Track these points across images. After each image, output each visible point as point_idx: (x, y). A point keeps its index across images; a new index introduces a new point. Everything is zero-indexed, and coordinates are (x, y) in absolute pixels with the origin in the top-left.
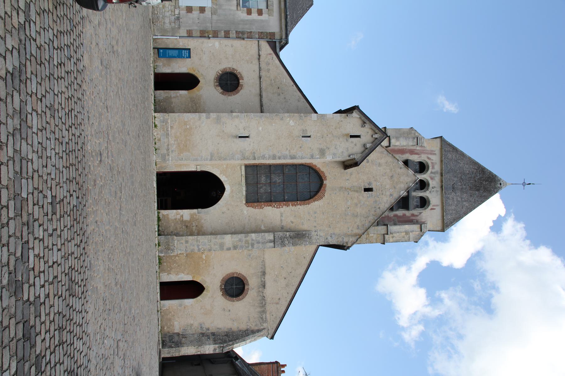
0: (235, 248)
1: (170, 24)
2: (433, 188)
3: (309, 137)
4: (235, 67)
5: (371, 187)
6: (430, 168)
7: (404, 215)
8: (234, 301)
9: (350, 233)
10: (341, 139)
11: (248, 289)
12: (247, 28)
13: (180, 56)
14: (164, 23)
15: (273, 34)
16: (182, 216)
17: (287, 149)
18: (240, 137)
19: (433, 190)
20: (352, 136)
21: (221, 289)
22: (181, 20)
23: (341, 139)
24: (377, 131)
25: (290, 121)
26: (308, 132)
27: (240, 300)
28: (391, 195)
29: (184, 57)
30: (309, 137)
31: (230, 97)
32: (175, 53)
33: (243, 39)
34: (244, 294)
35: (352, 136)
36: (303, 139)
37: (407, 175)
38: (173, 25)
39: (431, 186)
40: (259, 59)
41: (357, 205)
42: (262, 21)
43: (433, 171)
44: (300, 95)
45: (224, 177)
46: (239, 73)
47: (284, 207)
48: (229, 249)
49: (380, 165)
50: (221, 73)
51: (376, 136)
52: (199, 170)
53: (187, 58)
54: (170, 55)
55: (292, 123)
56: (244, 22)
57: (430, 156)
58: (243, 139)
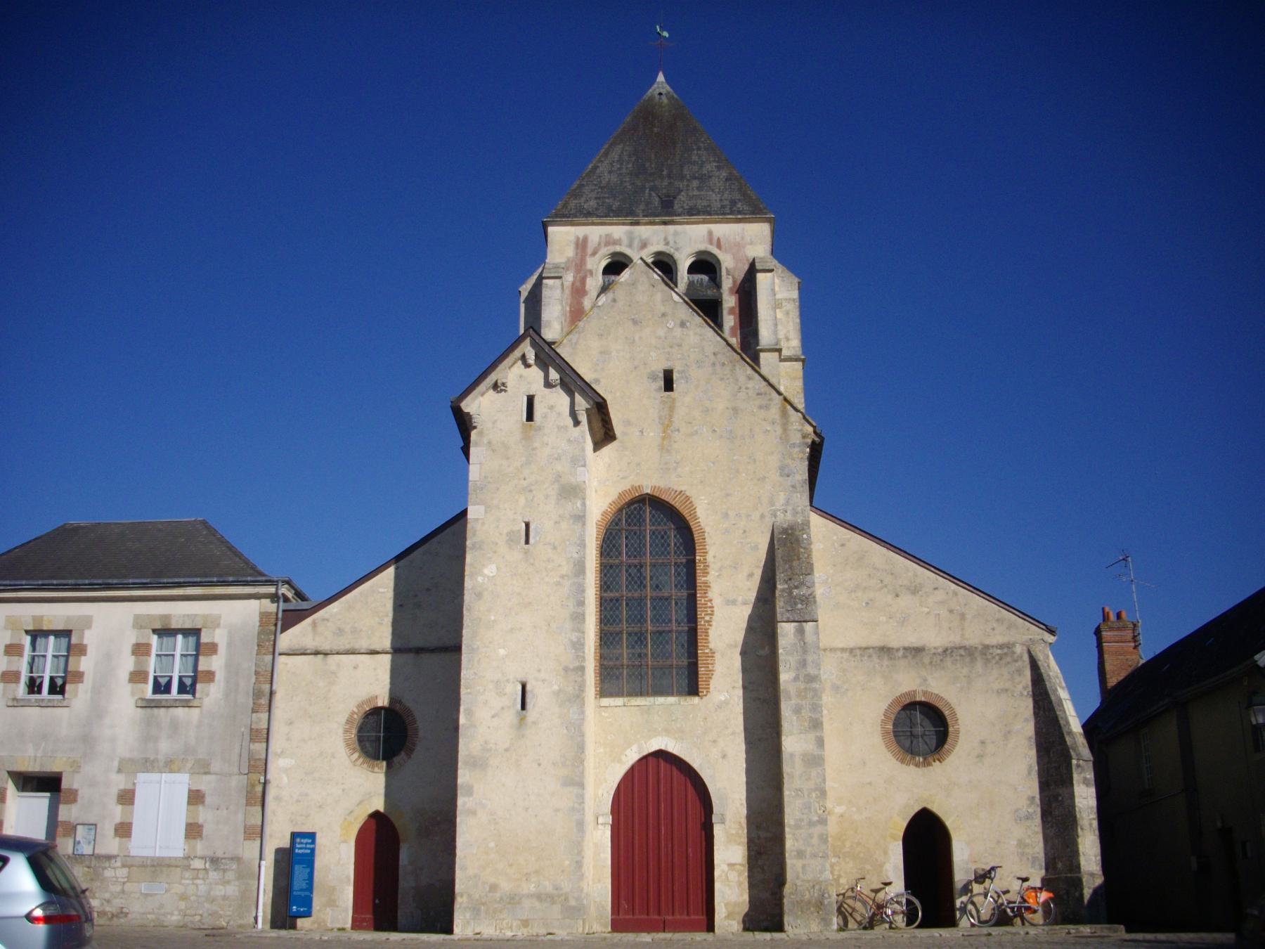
0: (816, 725)
1: (228, 882)
2: (667, 244)
3: (527, 525)
4: (343, 718)
5: (662, 375)
6: (618, 249)
7: (732, 329)
8: (957, 732)
9: (779, 430)
10: (536, 444)
11: (925, 693)
13: (309, 860)
14: (225, 898)
15: (264, 616)
16: (731, 865)
17: (558, 584)
18: (523, 707)
19: (672, 243)
20: (530, 417)
21: (926, 764)
22: (219, 854)
23: (536, 444)
24: (517, 353)
25: (484, 576)
26: (516, 528)
27: (954, 714)
28: (683, 324)
29: (313, 850)
30: (527, 525)
31: (421, 733)
32: (299, 872)
33: (272, 693)
34: (940, 705)
35: (530, 417)
36: (531, 540)
37: (634, 284)
38: (230, 875)
39: (661, 248)
40: (326, 654)
41: (707, 410)
44: (420, 550)
45: (628, 752)
46: (359, 706)
47: (710, 595)
48: (820, 742)
49: (605, 352)
50: (356, 755)
51: (531, 358)
52: (610, 819)
53: (313, 842)
54: (304, 886)
55: (490, 570)
57: (589, 251)
58: (528, 700)
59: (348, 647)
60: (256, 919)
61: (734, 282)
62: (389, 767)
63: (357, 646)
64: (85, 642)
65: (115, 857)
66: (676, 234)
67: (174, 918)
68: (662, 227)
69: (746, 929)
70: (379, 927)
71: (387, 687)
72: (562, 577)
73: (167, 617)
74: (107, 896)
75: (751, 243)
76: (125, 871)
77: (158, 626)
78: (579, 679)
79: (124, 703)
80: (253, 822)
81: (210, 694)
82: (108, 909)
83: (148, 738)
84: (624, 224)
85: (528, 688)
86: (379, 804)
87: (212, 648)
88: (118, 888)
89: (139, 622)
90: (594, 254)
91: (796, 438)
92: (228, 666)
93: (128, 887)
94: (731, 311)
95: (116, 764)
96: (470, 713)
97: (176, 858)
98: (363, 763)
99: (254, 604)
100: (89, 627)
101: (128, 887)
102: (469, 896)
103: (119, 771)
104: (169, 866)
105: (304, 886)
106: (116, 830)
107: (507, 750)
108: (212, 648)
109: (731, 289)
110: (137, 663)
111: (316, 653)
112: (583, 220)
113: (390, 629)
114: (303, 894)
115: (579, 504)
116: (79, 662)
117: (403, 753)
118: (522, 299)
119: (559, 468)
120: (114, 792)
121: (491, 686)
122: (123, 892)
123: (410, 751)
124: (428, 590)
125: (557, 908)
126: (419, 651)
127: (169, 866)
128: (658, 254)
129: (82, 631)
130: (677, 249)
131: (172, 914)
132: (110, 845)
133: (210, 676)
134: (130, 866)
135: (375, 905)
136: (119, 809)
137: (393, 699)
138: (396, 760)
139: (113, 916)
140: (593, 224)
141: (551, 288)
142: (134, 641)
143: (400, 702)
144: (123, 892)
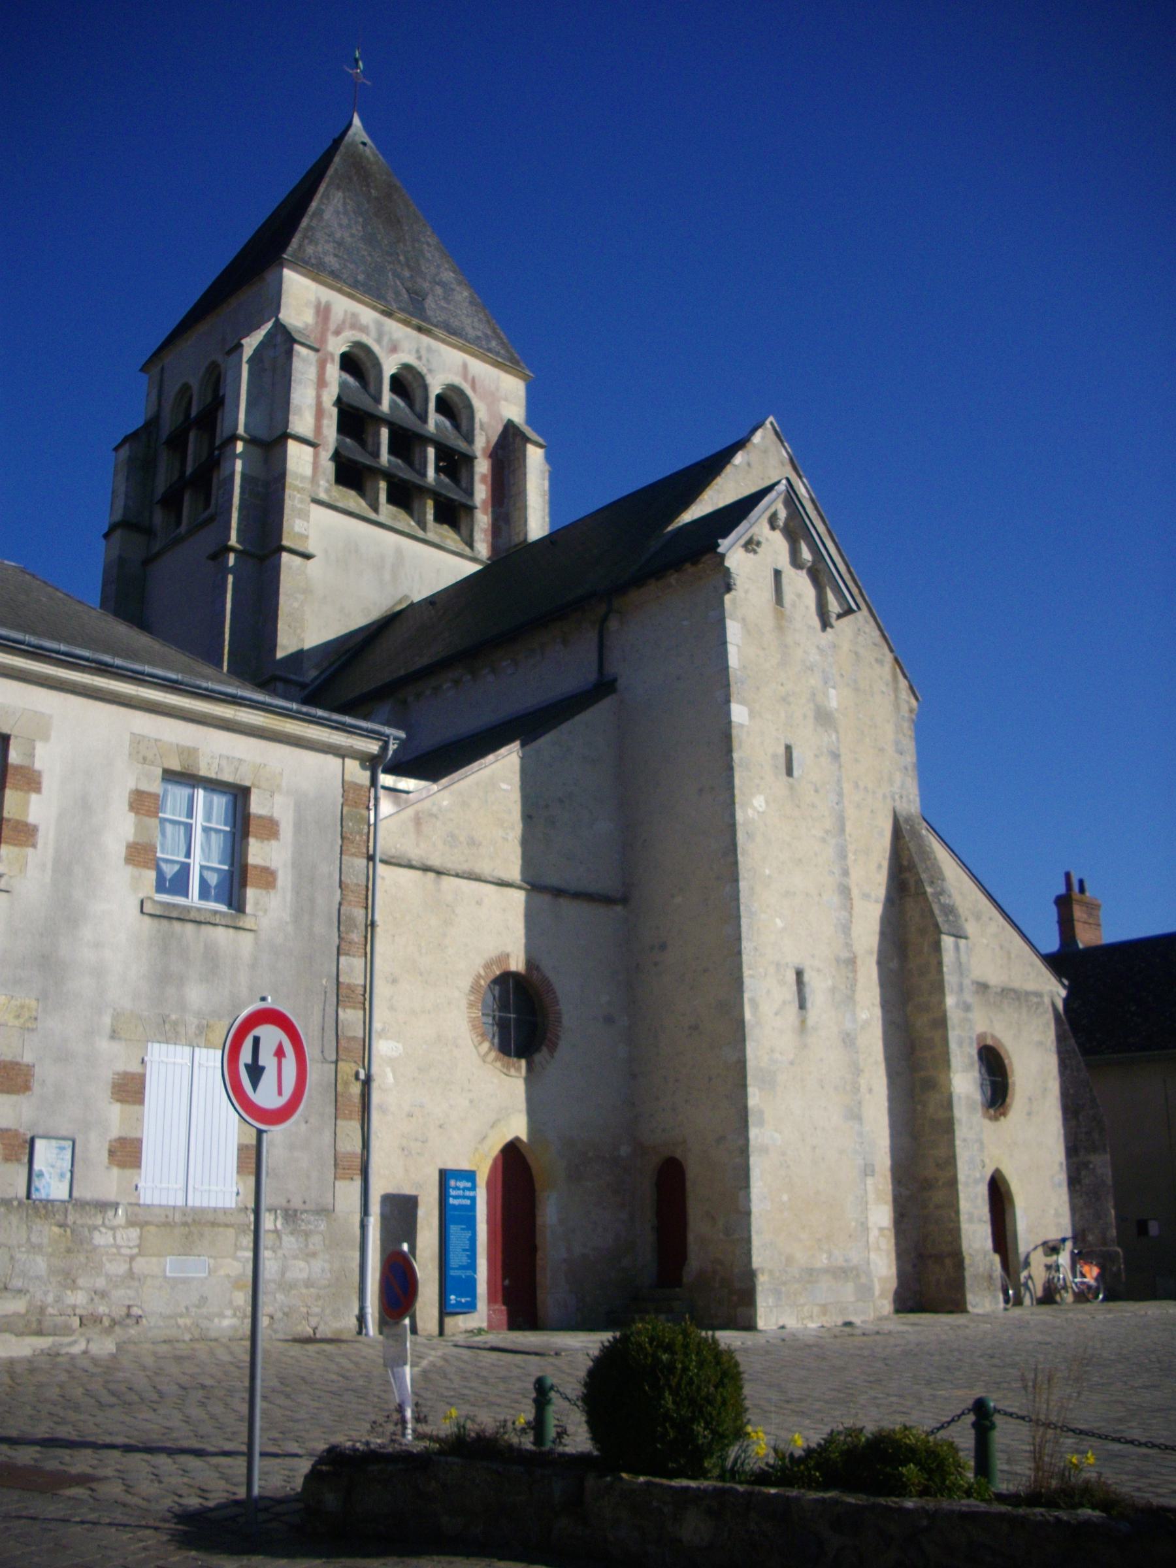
1: (314, 1255)
4: (466, 983)
12: (327, 899)
14: (308, 1284)
18: (802, 1006)
19: (424, 359)
22: (296, 1203)
25: (755, 809)
30: (788, 748)
31: (566, 1020)
38: (316, 1241)
39: (410, 359)
40: (439, 873)
42: (299, 827)
43: (373, 333)
50: (486, 1046)
54: (465, 1261)
55: (759, 802)
56: (303, 909)
57: (332, 326)
59: (464, 867)
60: (361, 1319)
61: (488, 442)
62: (530, 1069)
63: (477, 870)
64: (38, 766)
65: (116, 1206)
66: (429, 349)
67: (226, 1323)
68: (414, 333)
69: (898, 1311)
70: (513, 1325)
71: (522, 941)
72: (827, 832)
73: (190, 753)
74: (101, 1283)
75: (506, 400)
76: (134, 1233)
77: (175, 766)
78: (851, 975)
79: (118, 902)
80: (349, 1149)
81: (268, 907)
82: (102, 1309)
83: (164, 979)
84: (374, 308)
85: (806, 977)
86: (518, 1127)
87: (271, 829)
88: (122, 1268)
89: (140, 749)
90: (337, 333)
91: (905, 709)
92: (298, 864)
93: (140, 1265)
94: (484, 477)
95: (107, 1020)
96: (755, 1005)
97: (225, 1211)
98: (496, 1060)
99: (332, 763)
100: (46, 738)
101: (140, 1265)
102: (771, 1272)
103: (114, 1035)
104: (214, 1224)
105: (465, 1261)
106: (111, 1153)
107: (792, 1063)
108: (271, 829)
109: (484, 450)
110: (139, 828)
111: (426, 869)
112: (330, 281)
113: (518, 850)
114: (463, 1274)
115: (834, 737)
116: (26, 804)
117: (544, 1049)
118: (245, 358)
119: (812, 682)
120: (106, 1075)
121: (772, 970)
122: (131, 1274)
123: (553, 1048)
124: (561, 801)
125: (850, 1287)
126: (558, 892)
127: (214, 1224)
128: (407, 367)
129: (31, 743)
130: (430, 371)
131: (221, 1316)
132: (105, 1182)
133: (268, 878)
134: (142, 1225)
135: (504, 1288)
136: (115, 1112)
137: (530, 963)
138: (538, 1057)
139: (114, 1322)
140: (340, 291)
141: (305, 360)
142: (131, 784)
143: (538, 968)
144: (131, 1274)
